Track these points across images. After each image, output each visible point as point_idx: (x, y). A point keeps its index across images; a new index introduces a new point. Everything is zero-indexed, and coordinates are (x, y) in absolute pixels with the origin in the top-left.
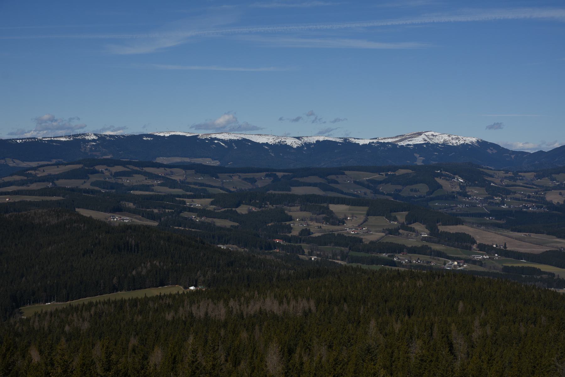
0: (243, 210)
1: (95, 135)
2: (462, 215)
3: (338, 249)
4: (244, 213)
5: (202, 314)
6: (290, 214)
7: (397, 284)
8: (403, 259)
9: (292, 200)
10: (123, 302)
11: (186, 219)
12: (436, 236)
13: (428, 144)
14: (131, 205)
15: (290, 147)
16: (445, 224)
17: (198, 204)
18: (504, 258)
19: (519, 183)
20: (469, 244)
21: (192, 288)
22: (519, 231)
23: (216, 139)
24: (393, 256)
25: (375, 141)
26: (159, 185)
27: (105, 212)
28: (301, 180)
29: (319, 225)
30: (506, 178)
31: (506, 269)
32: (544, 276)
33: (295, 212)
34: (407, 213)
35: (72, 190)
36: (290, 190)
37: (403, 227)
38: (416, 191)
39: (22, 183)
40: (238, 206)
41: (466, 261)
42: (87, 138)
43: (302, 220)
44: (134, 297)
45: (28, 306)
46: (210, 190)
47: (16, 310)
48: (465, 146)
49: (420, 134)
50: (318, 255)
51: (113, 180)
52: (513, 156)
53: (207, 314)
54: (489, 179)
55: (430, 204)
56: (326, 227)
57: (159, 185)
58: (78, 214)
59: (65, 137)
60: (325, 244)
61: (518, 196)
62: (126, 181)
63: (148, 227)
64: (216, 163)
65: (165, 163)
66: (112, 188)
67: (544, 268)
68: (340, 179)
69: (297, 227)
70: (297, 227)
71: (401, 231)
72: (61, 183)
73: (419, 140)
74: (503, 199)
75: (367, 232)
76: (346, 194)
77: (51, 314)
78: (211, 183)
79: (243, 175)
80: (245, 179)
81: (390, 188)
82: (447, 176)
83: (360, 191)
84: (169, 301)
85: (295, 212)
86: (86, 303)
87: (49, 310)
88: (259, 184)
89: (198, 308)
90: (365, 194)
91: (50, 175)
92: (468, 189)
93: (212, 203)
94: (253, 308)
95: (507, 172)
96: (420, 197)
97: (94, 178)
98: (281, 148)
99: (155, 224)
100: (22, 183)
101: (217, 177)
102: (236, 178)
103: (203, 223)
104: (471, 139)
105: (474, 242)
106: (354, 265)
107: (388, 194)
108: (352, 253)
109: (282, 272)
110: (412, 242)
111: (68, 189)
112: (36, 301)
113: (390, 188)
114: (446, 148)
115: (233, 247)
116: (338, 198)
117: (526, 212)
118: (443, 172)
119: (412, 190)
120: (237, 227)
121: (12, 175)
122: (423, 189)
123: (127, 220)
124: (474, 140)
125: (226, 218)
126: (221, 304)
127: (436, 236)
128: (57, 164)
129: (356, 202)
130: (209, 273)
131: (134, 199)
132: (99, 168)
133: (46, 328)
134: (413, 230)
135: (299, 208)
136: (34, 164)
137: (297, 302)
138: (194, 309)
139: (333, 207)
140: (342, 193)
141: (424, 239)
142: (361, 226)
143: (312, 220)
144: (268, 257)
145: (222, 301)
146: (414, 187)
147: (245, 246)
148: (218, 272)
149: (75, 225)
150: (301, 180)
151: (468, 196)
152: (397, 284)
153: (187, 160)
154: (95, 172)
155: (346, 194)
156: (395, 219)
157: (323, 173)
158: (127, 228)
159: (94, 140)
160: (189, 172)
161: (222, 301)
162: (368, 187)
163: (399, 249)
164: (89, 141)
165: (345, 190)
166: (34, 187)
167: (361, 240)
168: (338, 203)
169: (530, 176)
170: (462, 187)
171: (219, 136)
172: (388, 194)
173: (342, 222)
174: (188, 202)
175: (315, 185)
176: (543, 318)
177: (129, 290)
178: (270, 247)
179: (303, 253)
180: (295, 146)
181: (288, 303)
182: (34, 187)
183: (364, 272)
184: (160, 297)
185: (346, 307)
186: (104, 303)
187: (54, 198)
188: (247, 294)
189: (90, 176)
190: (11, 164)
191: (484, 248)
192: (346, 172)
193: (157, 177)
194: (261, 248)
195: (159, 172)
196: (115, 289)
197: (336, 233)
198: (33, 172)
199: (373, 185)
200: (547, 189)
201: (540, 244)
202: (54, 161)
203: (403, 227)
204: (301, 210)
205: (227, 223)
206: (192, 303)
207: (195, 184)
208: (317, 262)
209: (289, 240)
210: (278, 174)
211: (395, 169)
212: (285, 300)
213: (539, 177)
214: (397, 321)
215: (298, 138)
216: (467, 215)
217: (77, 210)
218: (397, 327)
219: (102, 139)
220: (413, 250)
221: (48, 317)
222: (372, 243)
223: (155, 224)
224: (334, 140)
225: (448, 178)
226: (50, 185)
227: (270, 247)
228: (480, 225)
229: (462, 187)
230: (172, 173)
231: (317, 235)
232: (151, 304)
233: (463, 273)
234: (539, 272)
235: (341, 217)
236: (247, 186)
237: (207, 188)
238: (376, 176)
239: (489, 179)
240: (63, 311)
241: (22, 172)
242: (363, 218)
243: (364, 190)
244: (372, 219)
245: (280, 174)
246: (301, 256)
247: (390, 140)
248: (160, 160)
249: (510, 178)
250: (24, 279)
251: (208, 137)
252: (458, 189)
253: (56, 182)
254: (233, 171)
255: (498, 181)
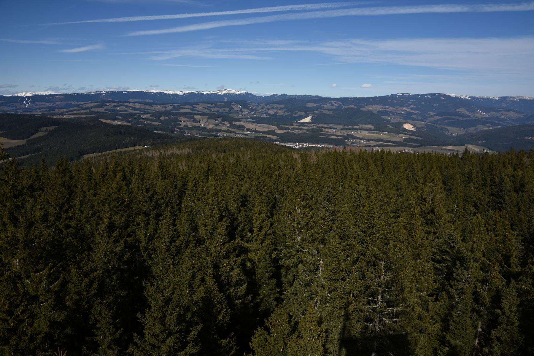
0: (162, 118)
1: (105, 91)
2: (241, 118)
3: (198, 131)
4: (163, 119)
5: (151, 155)
6: (180, 119)
7: (220, 142)
8: (220, 134)
9: (181, 114)
10: (121, 152)
11: (141, 122)
12: (232, 126)
13: (228, 93)
14: (120, 117)
15: (179, 95)
16: (235, 122)
17: (145, 116)
18: (255, 133)
19: (260, 107)
20: (243, 129)
21: (146, 147)
22: (260, 124)
23: (151, 92)
24: (218, 134)
25: (210, 92)
26: (130, 110)
27: (111, 120)
28: (183, 107)
29: (191, 123)
30: (255, 105)
31: (256, 137)
32: (268, 139)
33: (182, 118)
34: (221, 118)
35: (97, 112)
36: (179, 111)
37: (221, 123)
38: (224, 110)
39: (78, 110)
40: (160, 117)
41: (243, 134)
42: (101, 92)
43: (185, 121)
44: (125, 150)
45: (85, 155)
46: (150, 111)
47: (81, 157)
48: (241, 94)
49: (225, 90)
50: (191, 134)
51: (113, 108)
52: (257, 98)
53: (152, 155)
54: (250, 106)
55: (230, 115)
56: (193, 124)
57: (130, 110)
58: (101, 121)
59: (93, 92)
60: (193, 130)
61: (259, 111)
62: (118, 109)
63: (127, 125)
64: (152, 101)
65: (132, 101)
66: (113, 111)
67: (268, 136)
68: (197, 106)
69: (183, 124)
70: (183, 124)
71: (220, 124)
72: (93, 110)
73: (225, 92)
74: (254, 113)
75: (208, 125)
76: (200, 112)
77: (95, 158)
78: (150, 109)
79: (162, 106)
80: (163, 107)
81: (215, 109)
82: (235, 105)
83: (205, 111)
84: (138, 151)
85: (182, 118)
86: (107, 153)
87: (94, 156)
88: (168, 109)
89: (149, 153)
90: (207, 111)
91: (88, 107)
92: (242, 109)
93: (151, 116)
94: (169, 152)
95: (255, 103)
96: (226, 112)
97: (105, 108)
98: (176, 95)
99: (130, 124)
100: (78, 110)
101: (152, 107)
102: (159, 107)
103: (148, 123)
104: (243, 92)
105: (245, 128)
106: (204, 137)
107: (215, 112)
108: (203, 133)
109: (179, 140)
110: (224, 128)
111: (96, 112)
112: (88, 154)
113: (215, 109)
114: (235, 95)
115: (160, 132)
116: (197, 113)
117: (262, 117)
118: (234, 104)
119: (223, 110)
120: (160, 125)
121: (74, 107)
122: (227, 109)
123: (119, 123)
124: (244, 92)
125: (156, 121)
126: (158, 151)
127: (232, 126)
128: (91, 103)
129: (204, 114)
130: (152, 141)
131: (121, 115)
132: (107, 104)
133: (93, 162)
134: (224, 124)
135: (183, 117)
136: (82, 103)
137: (185, 149)
138: (148, 153)
139: (195, 117)
140: (198, 111)
141: (228, 127)
142: (206, 123)
143: (188, 121)
144: (173, 135)
145: (158, 150)
146: (224, 109)
147: (164, 131)
148: (155, 141)
149: (100, 125)
150: (183, 107)
151: (243, 112)
152: (220, 142)
153: (140, 100)
154: (106, 105)
155: (200, 112)
156: (218, 120)
157: (191, 104)
158: (119, 125)
159: (104, 93)
160: (141, 105)
161: (158, 150)
162: (208, 109)
163: (220, 131)
164: (102, 94)
165: (199, 110)
166: (83, 111)
167: (206, 128)
168: (197, 115)
169: (263, 105)
170: (241, 109)
171: (152, 91)
172: (215, 112)
173: (199, 122)
174: (142, 116)
175: (188, 109)
176: (269, 151)
177: (122, 148)
178: (173, 131)
179: (185, 133)
180: (181, 95)
181: (182, 150)
182: (83, 111)
183: (208, 139)
184: (135, 150)
185: (203, 150)
186: (114, 153)
187: (91, 116)
188: (167, 148)
189: (104, 107)
190: (73, 103)
191: (248, 130)
192: (200, 104)
193: (129, 107)
194: (170, 132)
195: (130, 105)
196: (117, 148)
197: (197, 126)
198: (82, 106)
199: (209, 108)
200: (269, 109)
201: (267, 128)
202: (89, 102)
203: (221, 123)
204: (184, 118)
205: (157, 123)
206: (147, 152)
207: (144, 109)
208: (190, 136)
209: (180, 129)
210: (175, 105)
211: (217, 102)
212: (181, 149)
213: (266, 105)
214: (221, 154)
215: (182, 92)
216: (243, 118)
217: (100, 120)
218: (222, 156)
219: (107, 93)
220: (224, 131)
221: (93, 159)
222: (210, 129)
223: (130, 124)
224: (195, 92)
225: (236, 106)
226: (89, 111)
227: (173, 131)
228: (247, 122)
229: (241, 109)
230: (135, 105)
231: (190, 127)
232: (131, 153)
233: (242, 138)
234: (266, 137)
235: (199, 120)
236: (164, 110)
237: (149, 111)
238: (210, 105)
239: (250, 106)
240: (99, 156)
241: (78, 106)
242: (206, 120)
243: (206, 110)
244: (209, 120)
245: (175, 105)
246: (185, 134)
247: (215, 92)
248: (130, 100)
249: (257, 105)
250: (82, 146)
251: (148, 91)
252: (239, 109)
253: (91, 109)
254: (158, 104)
255: (253, 106)
